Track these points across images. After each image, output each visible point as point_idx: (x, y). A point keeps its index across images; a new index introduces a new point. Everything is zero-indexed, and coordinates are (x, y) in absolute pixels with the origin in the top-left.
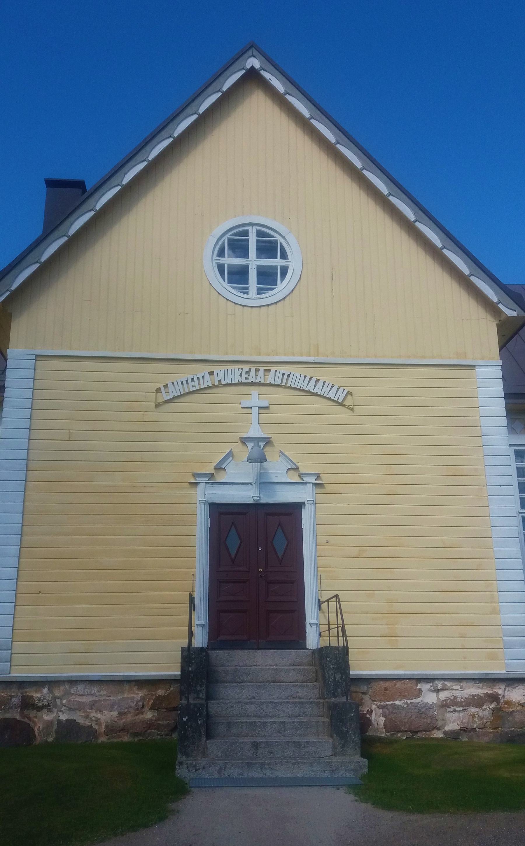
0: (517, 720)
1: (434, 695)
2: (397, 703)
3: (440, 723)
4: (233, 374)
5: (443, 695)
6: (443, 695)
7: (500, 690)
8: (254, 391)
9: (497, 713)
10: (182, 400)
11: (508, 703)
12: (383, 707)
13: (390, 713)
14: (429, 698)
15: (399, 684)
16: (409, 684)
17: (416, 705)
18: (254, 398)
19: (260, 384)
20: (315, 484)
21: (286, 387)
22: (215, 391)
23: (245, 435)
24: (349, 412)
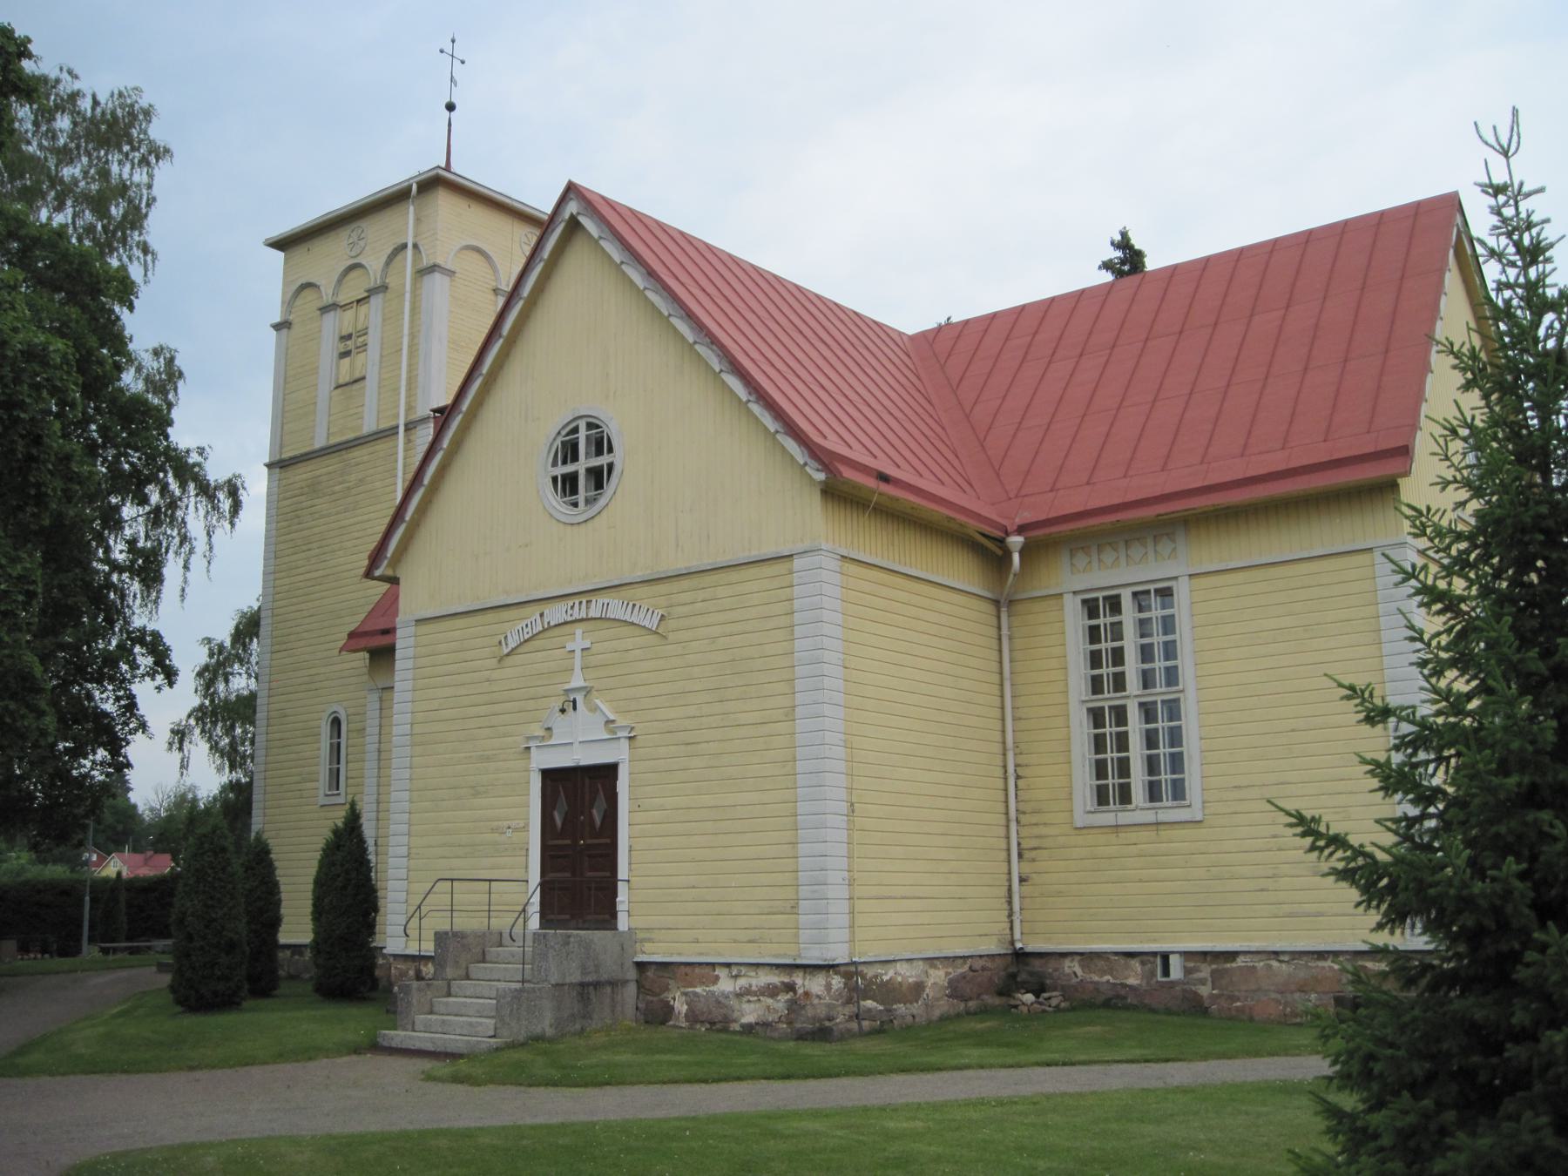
0: (1514, 1020)
1: (731, 982)
2: (698, 990)
3: (736, 1014)
4: (556, 613)
5: (742, 982)
6: (742, 982)
7: (798, 979)
8: (579, 630)
9: (794, 1006)
10: (520, 650)
11: (807, 994)
12: (686, 994)
13: (691, 1000)
14: (725, 985)
15: (697, 970)
16: (707, 970)
17: (713, 993)
18: (579, 639)
19: (582, 620)
20: (630, 738)
21: (550, 628)
22: (547, 634)
23: (567, 687)
24: (652, 639)
